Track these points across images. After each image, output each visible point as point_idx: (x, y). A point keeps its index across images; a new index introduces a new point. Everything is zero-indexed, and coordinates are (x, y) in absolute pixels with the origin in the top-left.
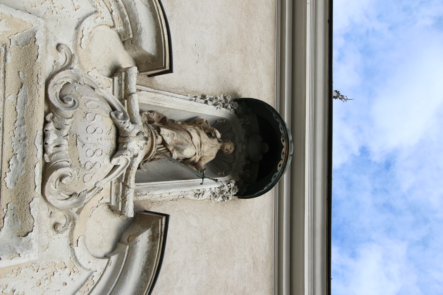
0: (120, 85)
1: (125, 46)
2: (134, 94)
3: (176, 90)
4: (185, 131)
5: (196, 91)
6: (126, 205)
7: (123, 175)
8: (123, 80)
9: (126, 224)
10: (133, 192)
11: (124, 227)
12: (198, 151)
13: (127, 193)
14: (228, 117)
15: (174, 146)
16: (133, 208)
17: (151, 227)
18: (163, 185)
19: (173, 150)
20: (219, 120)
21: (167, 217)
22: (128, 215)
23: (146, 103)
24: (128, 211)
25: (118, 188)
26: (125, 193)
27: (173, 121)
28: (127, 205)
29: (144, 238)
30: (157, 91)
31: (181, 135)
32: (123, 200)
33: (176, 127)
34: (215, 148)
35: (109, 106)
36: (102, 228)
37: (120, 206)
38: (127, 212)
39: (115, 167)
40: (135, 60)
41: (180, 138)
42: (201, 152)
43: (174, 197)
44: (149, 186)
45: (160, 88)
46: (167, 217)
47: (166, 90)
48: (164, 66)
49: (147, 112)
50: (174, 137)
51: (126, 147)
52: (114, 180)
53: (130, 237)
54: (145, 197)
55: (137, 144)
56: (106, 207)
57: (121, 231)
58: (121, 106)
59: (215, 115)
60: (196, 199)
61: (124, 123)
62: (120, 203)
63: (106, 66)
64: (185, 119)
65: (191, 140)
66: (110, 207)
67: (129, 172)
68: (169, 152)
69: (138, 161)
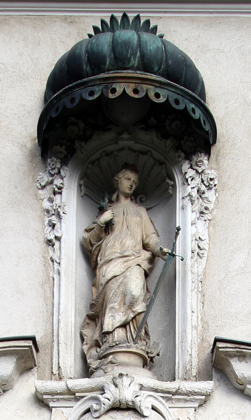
0: (58, 400)
1: (8, 389)
2: (68, 386)
3: (49, 301)
4: (105, 288)
5: (43, 259)
6: (198, 391)
7: (164, 396)
8: (53, 397)
9: (224, 381)
10: (184, 382)
11: (226, 384)
12: (134, 259)
13: (185, 390)
14: (77, 174)
15: (128, 310)
16: (203, 382)
17: (228, 359)
18: (181, 323)
19: (133, 312)
20: (81, 191)
21: (217, 340)
22: (211, 389)
23: (73, 356)
24: (206, 389)
25: (179, 400)
26: (184, 393)
27: (92, 306)
28: (199, 389)
29: (241, 367)
30: (55, 338)
31: (112, 297)
32: (192, 394)
33: (100, 301)
34: (129, 218)
35: (85, 415)
36: (223, 415)
37: (199, 398)
38: (207, 390)
39: (154, 408)
40: (22, 374)
41: (116, 298)
42: (135, 254)
43: (199, 301)
44: (180, 347)
45: (50, 330)
46: (217, 340)
47: (52, 320)
48: (28, 348)
49: (84, 346)
50: (116, 307)
51: (131, 402)
52: (168, 405)
53: (238, 382)
54: (194, 355)
55: (128, 388)
56: (200, 410)
57: (232, 389)
58: (84, 401)
59: (75, 213)
60: (206, 255)
61: (104, 404)
62: (196, 398)
63: (37, 414)
64: (85, 266)
65: (117, 278)
66: (200, 406)
67: (161, 390)
68: (136, 317)
69: (147, 381)
